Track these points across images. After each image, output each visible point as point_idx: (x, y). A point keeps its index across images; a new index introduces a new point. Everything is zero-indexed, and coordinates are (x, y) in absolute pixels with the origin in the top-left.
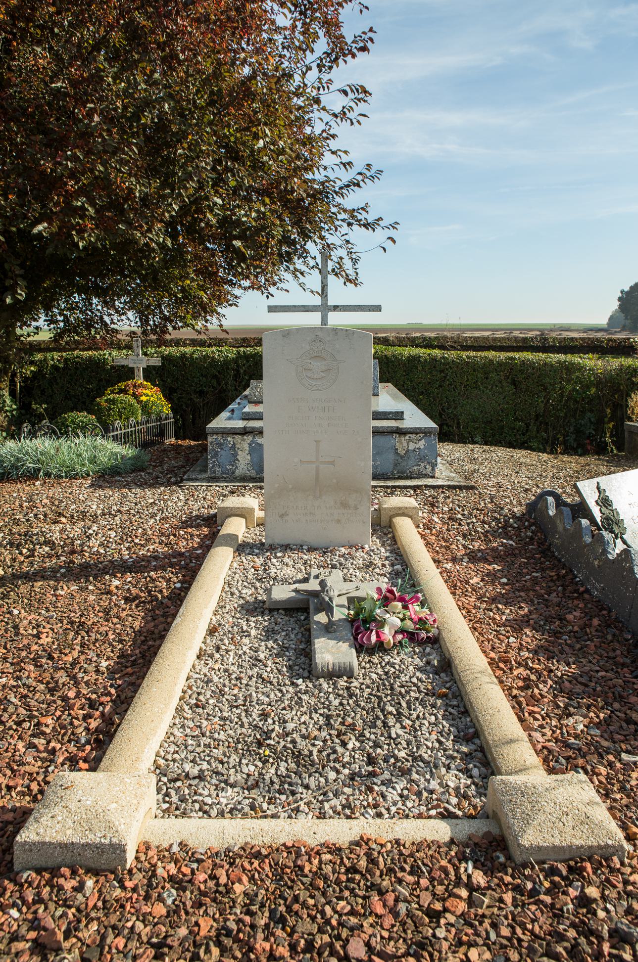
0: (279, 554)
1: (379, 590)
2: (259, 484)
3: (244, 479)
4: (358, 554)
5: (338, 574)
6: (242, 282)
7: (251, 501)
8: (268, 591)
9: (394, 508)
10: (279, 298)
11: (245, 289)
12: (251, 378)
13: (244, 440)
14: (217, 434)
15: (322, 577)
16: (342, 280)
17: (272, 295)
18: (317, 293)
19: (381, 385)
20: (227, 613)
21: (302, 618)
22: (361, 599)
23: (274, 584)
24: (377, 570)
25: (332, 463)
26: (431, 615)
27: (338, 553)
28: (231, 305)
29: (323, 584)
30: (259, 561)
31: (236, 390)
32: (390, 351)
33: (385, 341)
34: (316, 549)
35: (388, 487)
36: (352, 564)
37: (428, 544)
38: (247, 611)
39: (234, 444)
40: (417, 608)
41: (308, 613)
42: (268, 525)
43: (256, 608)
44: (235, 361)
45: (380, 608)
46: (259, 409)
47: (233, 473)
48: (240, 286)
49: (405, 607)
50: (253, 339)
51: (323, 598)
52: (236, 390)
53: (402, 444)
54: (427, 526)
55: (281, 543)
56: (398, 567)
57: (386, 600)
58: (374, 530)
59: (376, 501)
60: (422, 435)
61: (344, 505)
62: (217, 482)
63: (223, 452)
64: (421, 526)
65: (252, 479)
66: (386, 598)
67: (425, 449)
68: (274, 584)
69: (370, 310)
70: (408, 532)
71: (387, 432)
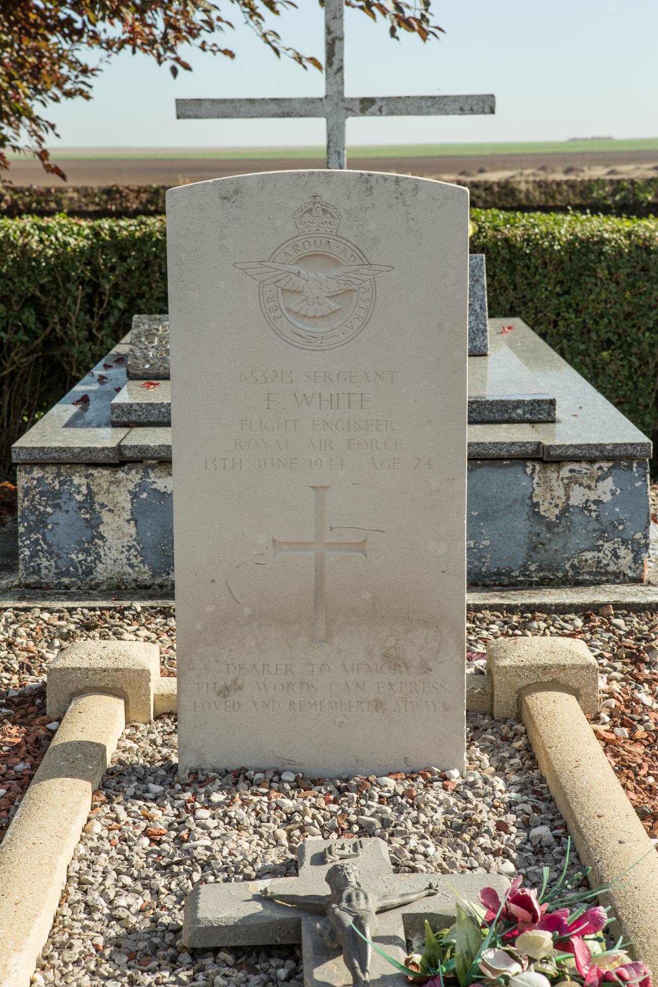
0: (217, 797)
1: (490, 896)
2: (159, 603)
3: (119, 589)
4: (431, 796)
5: (378, 850)
6: (100, 26)
7: (139, 651)
8: (188, 900)
9: (531, 668)
10: (208, 77)
11: (109, 45)
12: (133, 308)
13: (117, 483)
14: (43, 465)
15: (334, 859)
16: (384, 23)
17: (187, 67)
18: (313, 60)
19: (492, 325)
20: (77, 963)
21: (282, 973)
22: (441, 921)
23: (204, 881)
24: (485, 840)
25: (361, 547)
26: (635, 966)
27: (376, 791)
28: (69, 94)
29: (337, 878)
30: (162, 817)
31: (91, 338)
32: (520, 226)
33: (505, 198)
34: (317, 782)
35: (511, 609)
36: (416, 822)
37: (623, 768)
38: (132, 956)
39: (90, 494)
40: (596, 948)
41: (298, 961)
42: (186, 716)
43: (157, 947)
44: (88, 257)
45: (493, 945)
46: (159, 394)
47: (89, 571)
48: (95, 37)
49: (563, 945)
50: (134, 196)
51: (338, 919)
52: (91, 338)
53: (551, 490)
54: (621, 719)
55: (223, 765)
56: (543, 831)
57: (510, 925)
58: (476, 728)
59: (480, 648)
60: (606, 465)
61: (394, 661)
62: (44, 597)
63: (59, 517)
64: (605, 716)
65: (142, 590)
66: (508, 919)
67: (615, 502)
68: (204, 881)
69: (462, 111)
70: (569, 733)
71: (509, 457)
